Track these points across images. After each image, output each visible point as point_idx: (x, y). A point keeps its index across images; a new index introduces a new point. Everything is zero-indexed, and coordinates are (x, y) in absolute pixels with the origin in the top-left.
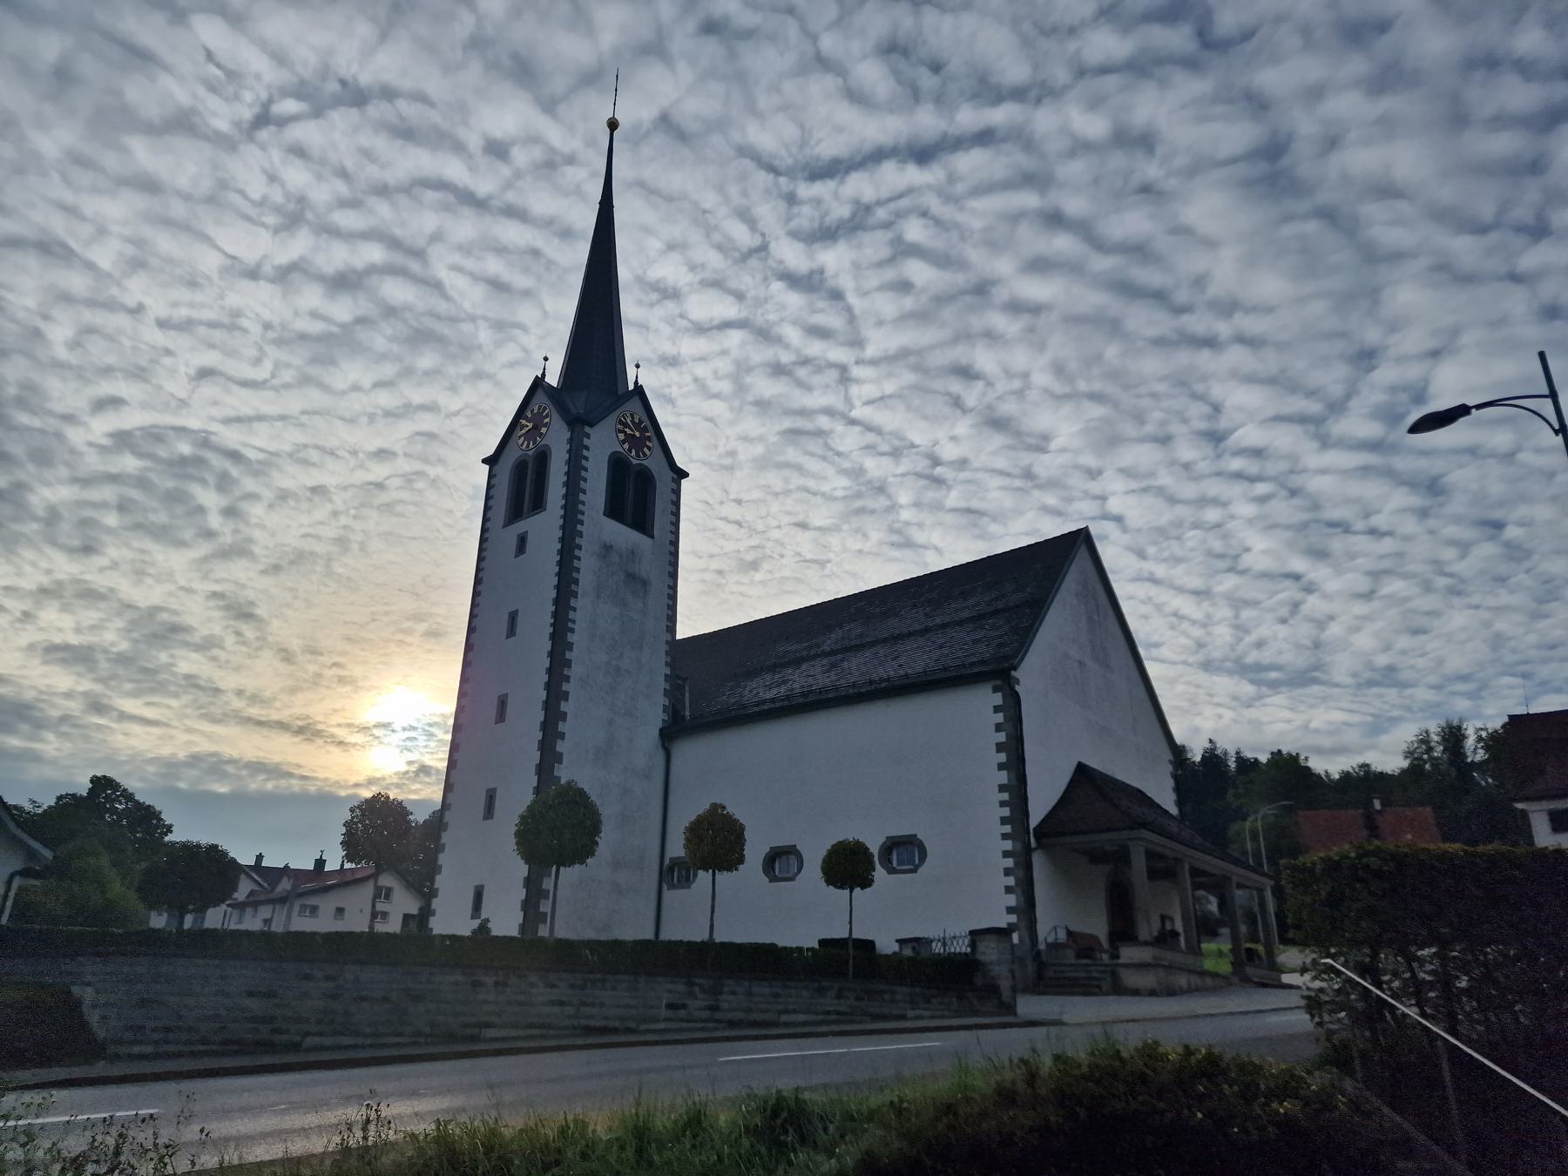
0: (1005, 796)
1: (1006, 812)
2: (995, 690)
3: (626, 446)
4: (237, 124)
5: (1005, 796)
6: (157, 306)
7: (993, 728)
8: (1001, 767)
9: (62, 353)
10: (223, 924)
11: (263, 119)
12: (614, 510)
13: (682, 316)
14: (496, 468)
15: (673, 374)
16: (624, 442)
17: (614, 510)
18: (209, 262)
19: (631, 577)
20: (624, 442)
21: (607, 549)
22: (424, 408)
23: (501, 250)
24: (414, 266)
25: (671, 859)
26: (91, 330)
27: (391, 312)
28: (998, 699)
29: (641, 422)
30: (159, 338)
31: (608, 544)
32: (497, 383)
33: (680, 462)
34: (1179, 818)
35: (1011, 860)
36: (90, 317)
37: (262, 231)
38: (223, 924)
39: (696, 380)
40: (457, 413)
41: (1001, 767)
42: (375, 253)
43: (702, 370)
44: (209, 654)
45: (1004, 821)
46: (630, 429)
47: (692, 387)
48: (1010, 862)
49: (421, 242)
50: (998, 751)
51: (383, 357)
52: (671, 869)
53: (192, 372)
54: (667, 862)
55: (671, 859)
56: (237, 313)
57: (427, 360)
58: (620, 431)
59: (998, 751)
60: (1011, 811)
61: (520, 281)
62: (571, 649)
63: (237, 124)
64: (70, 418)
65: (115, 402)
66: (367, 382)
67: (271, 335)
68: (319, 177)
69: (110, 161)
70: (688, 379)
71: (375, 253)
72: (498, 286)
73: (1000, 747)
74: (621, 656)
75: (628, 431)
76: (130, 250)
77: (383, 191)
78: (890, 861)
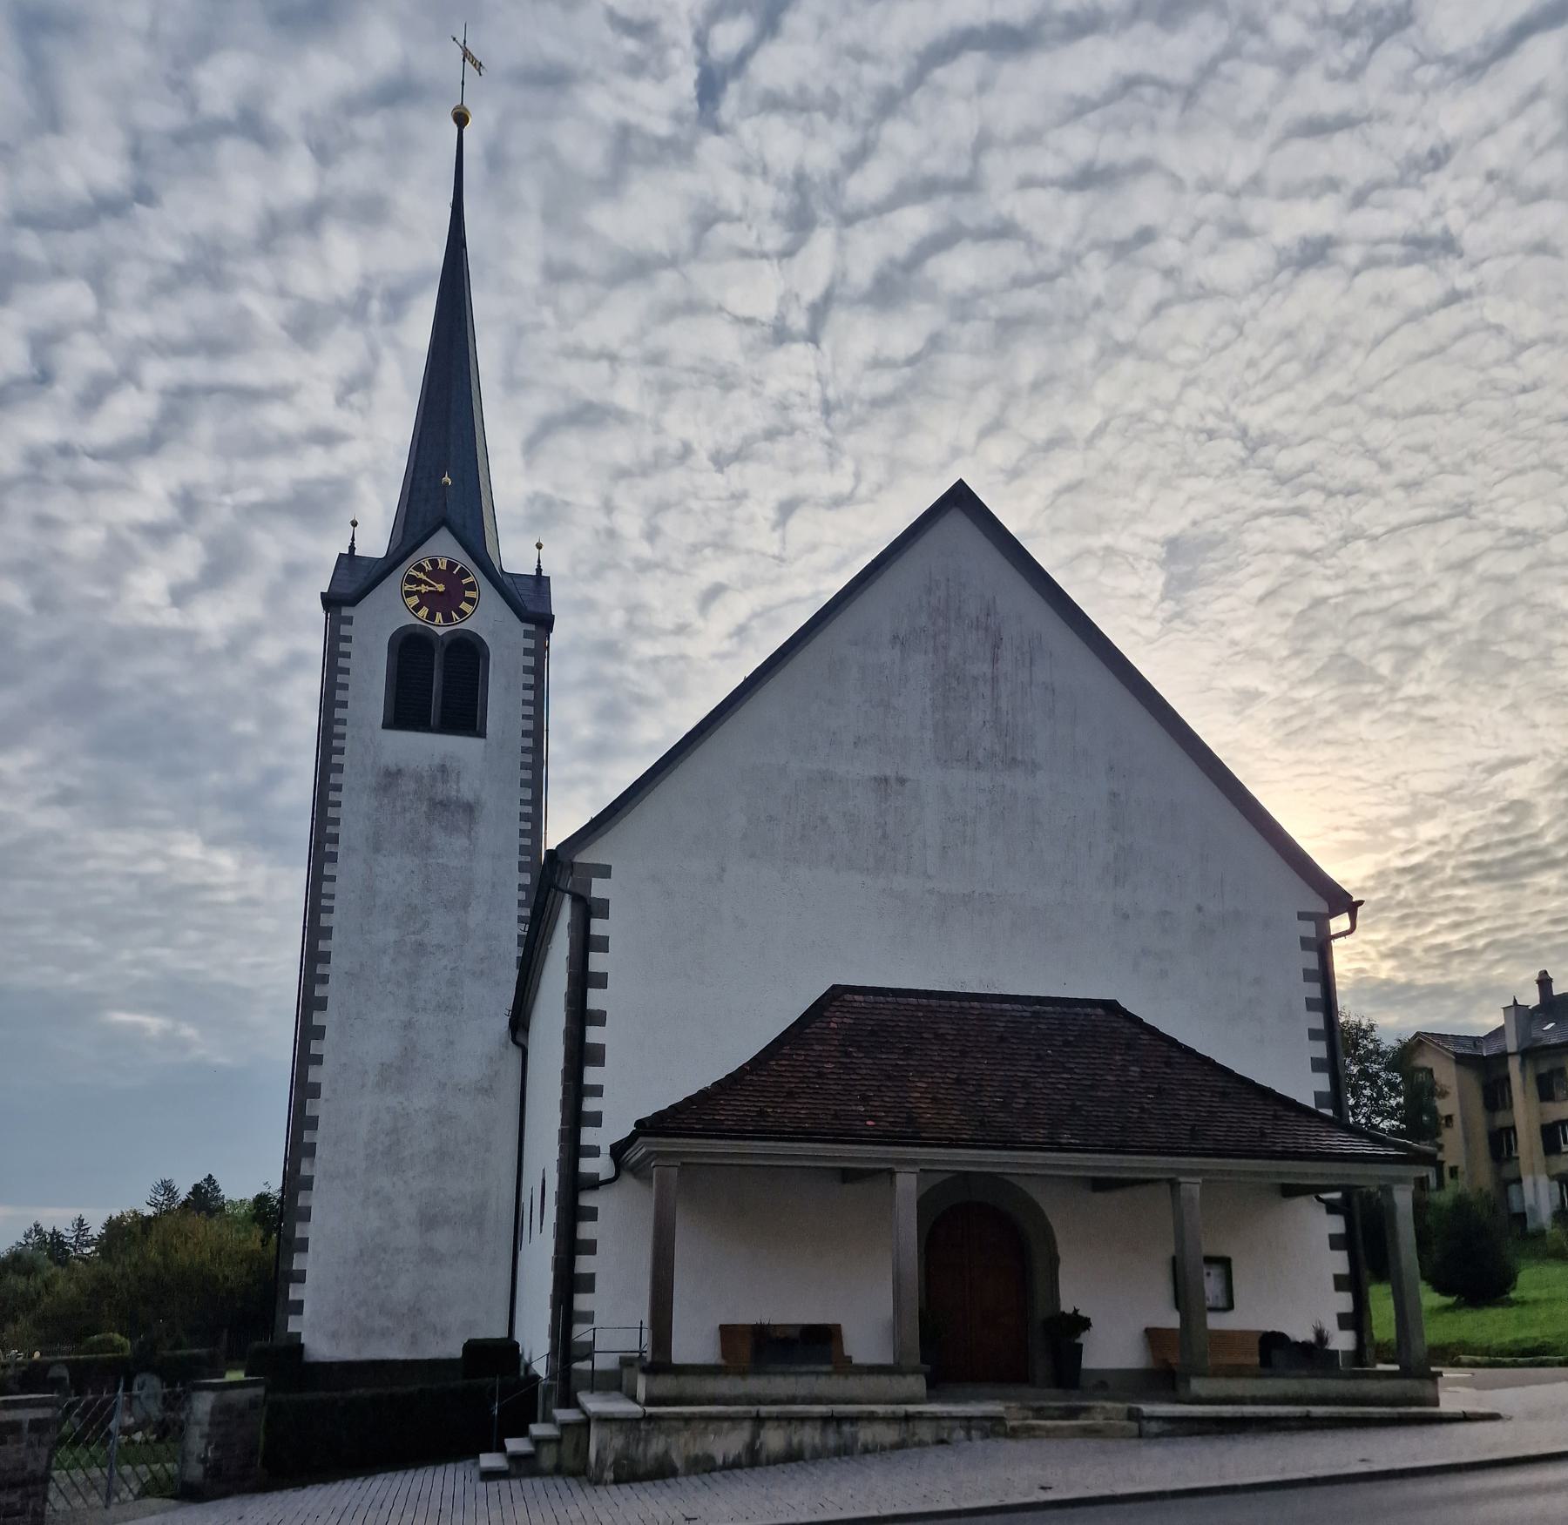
3: (424, 612)
4: (678, 117)
6: (705, 440)
9: (644, 550)
10: (1535, 1185)
11: (710, 86)
13: (1424, 60)
15: (1442, 184)
16: (417, 608)
18: (724, 343)
19: (441, 806)
20: (417, 608)
21: (391, 777)
22: (1053, 444)
23: (1079, 108)
24: (970, 212)
26: (662, 507)
27: (963, 307)
29: (452, 565)
30: (716, 483)
31: (393, 768)
32: (1143, 356)
36: (651, 487)
37: (764, 264)
38: (1535, 1185)
39: (1491, 176)
40: (1100, 431)
42: (916, 221)
43: (1493, 154)
44: (1357, 819)
46: (427, 584)
47: (1489, 192)
49: (962, 170)
51: (975, 386)
53: (772, 515)
56: (783, 407)
57: (1029, 361)
58: (409, 594)
61: (1114, 149)
63: (678, 117)
64: (681, 629)
65: (714, 593)
66: (969, 439)
67: (838, 418)
68: (810, 133)
69: (583, 255)
70: (1474, 184)
71: (916, 221)
72: (1088, 178)
74: (427, 924)
75: (424, 589)
76: (651, 373)
77: (889, 103)
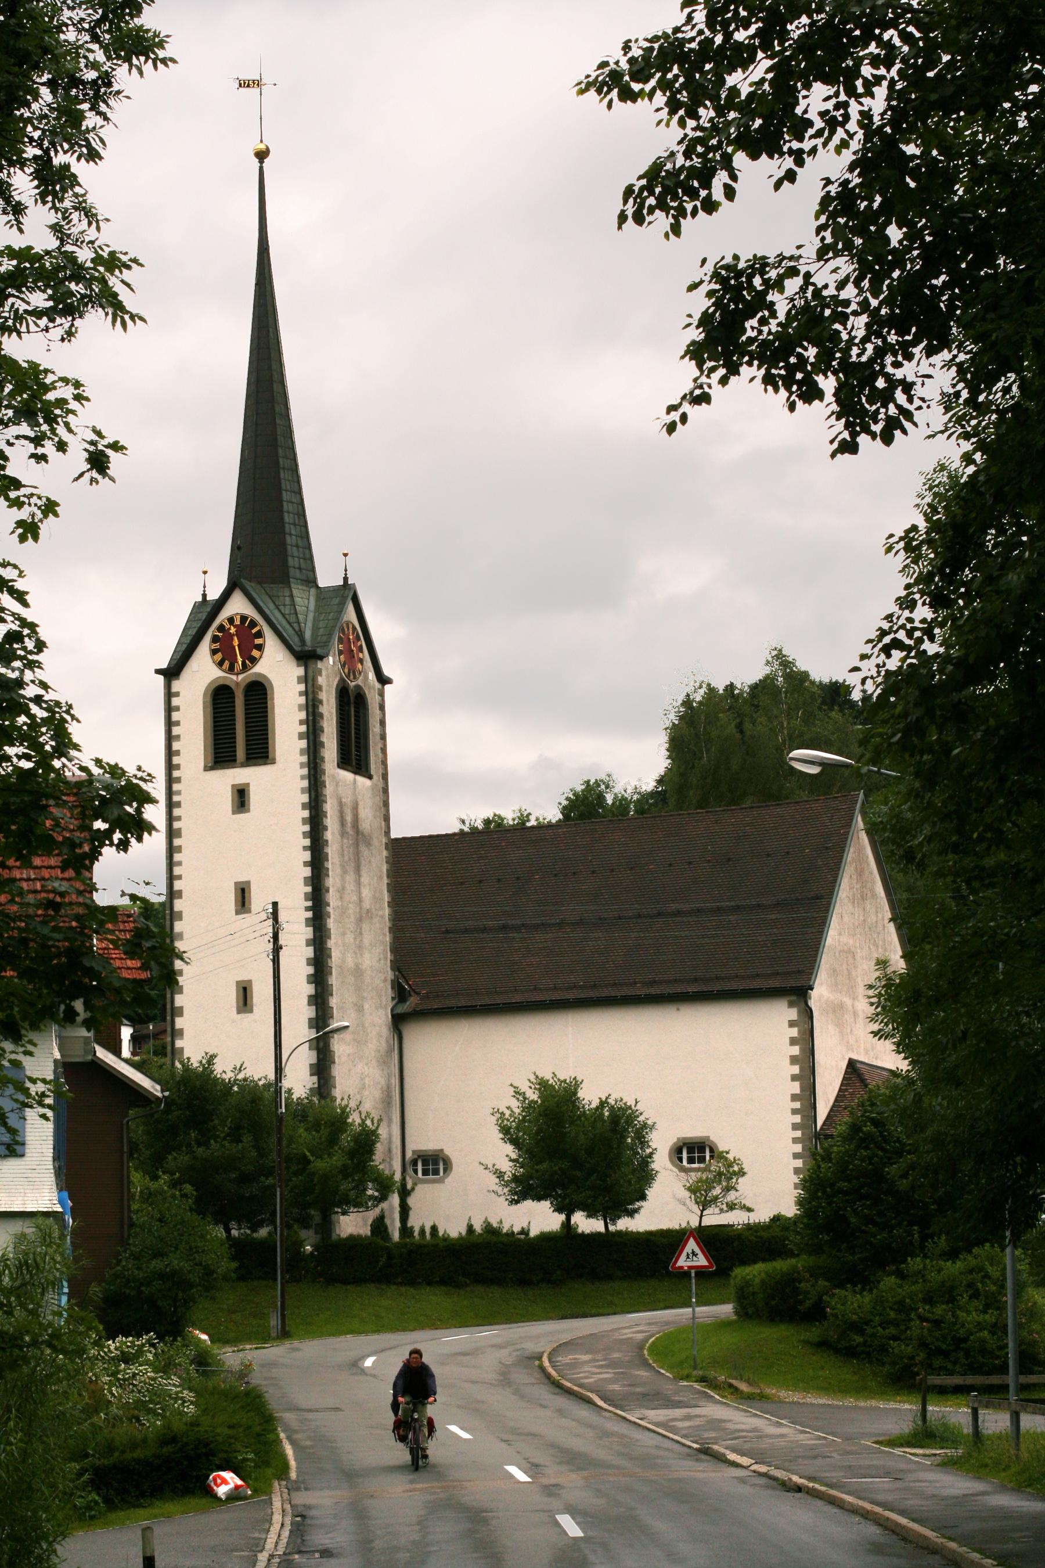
0: (797, 1105)
1: (797, 1119)
2: (791, 1005)
5: (797, 1105)
7: (788, 1041)
8: (794, 1078)
12: (344, 762)
14: (176, 686)
17: (344, 762)
25: (414, 1152)
28: (793, 1014)
33: (387, 671)
34: (48, 761)
35: (800, 1146)
41: (794, 1078)
45: (795, 1127)
48: (797, 1119)
50: (180, 847)
52: (414, 1163)
54: (409, 1155)
55: (414, 1152)
59: (180, 847)
60: (801, 1069)
62: (307, 920)
73: (794, 1060)
78: (681, 1160)
